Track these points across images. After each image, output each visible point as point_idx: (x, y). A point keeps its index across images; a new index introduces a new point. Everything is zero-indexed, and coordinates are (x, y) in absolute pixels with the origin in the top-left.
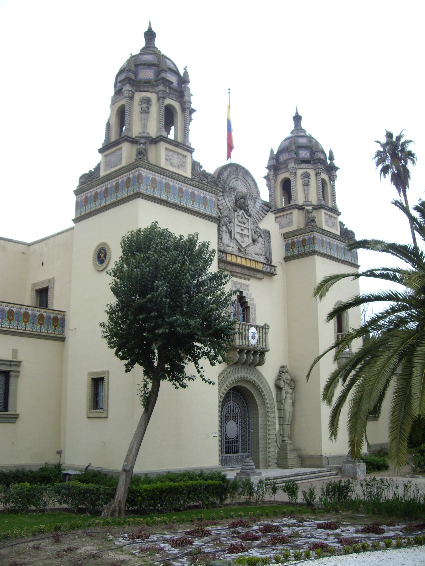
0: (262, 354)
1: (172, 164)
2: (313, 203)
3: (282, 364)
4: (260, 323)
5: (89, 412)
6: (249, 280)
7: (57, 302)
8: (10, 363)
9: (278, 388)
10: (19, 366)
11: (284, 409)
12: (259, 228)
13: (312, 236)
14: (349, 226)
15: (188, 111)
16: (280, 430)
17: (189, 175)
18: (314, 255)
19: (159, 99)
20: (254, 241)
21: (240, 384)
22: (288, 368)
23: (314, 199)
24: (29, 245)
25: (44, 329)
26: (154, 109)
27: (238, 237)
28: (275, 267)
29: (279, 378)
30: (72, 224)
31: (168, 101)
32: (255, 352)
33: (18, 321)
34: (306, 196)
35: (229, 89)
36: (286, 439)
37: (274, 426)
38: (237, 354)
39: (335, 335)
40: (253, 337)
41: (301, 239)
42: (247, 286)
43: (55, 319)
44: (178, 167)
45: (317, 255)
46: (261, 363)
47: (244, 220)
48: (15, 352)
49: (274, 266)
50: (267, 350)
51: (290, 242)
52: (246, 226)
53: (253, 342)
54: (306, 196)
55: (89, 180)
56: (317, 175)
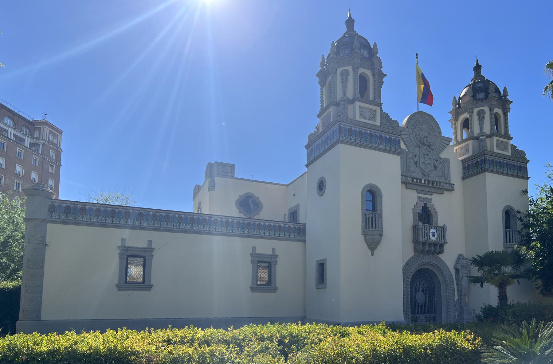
0: (442, 246)
1: (365, 118)
2: (487, 133)
3: (461, 253)
4: (440, 224)
5: (317, 285)
6: (431, 195)
7: (301, 220)
8: (270, 256)
9: (457, 270)
10: (276, 258)
11: (461, 285)
12: (440, 158)
13: (483, 158)
14: (519, 147)
15: (380, 76)
16: (458, 299)
17: (509, 154)
18: (484, 171)
19: (354, 70)
20: (435, 167)
21: (426, 267)
22: (464, 255)
23: (487, 129)
24: (287, 186)
25: (262, 233)
26: (487, 116)
27: (422, 166)
28: (454, 185)
29: (457, 262)
30: (306, 169)
31: (361, 71)
32: (435, 245)
33: (75, 214)
34: (481, 129)
35: (417, 55)
36: (463, 305)
37: (454, 295)
38: (421, 246)
39: (504, 231)
40: (433, 235)
41: (475, 162)
42: (431, 199)
43: (299, 229)
44: (370, 119)
45: (341, 143)
46: (441, 252)
47: (428, 152)
48: (150, 242)
49: (452, 184)
50: (446, 243)
51: (466, 165)
52: (429, 157)
53: (433, 239)
54: (481, 129)
55: (312, 140)
56: (490, 110)
